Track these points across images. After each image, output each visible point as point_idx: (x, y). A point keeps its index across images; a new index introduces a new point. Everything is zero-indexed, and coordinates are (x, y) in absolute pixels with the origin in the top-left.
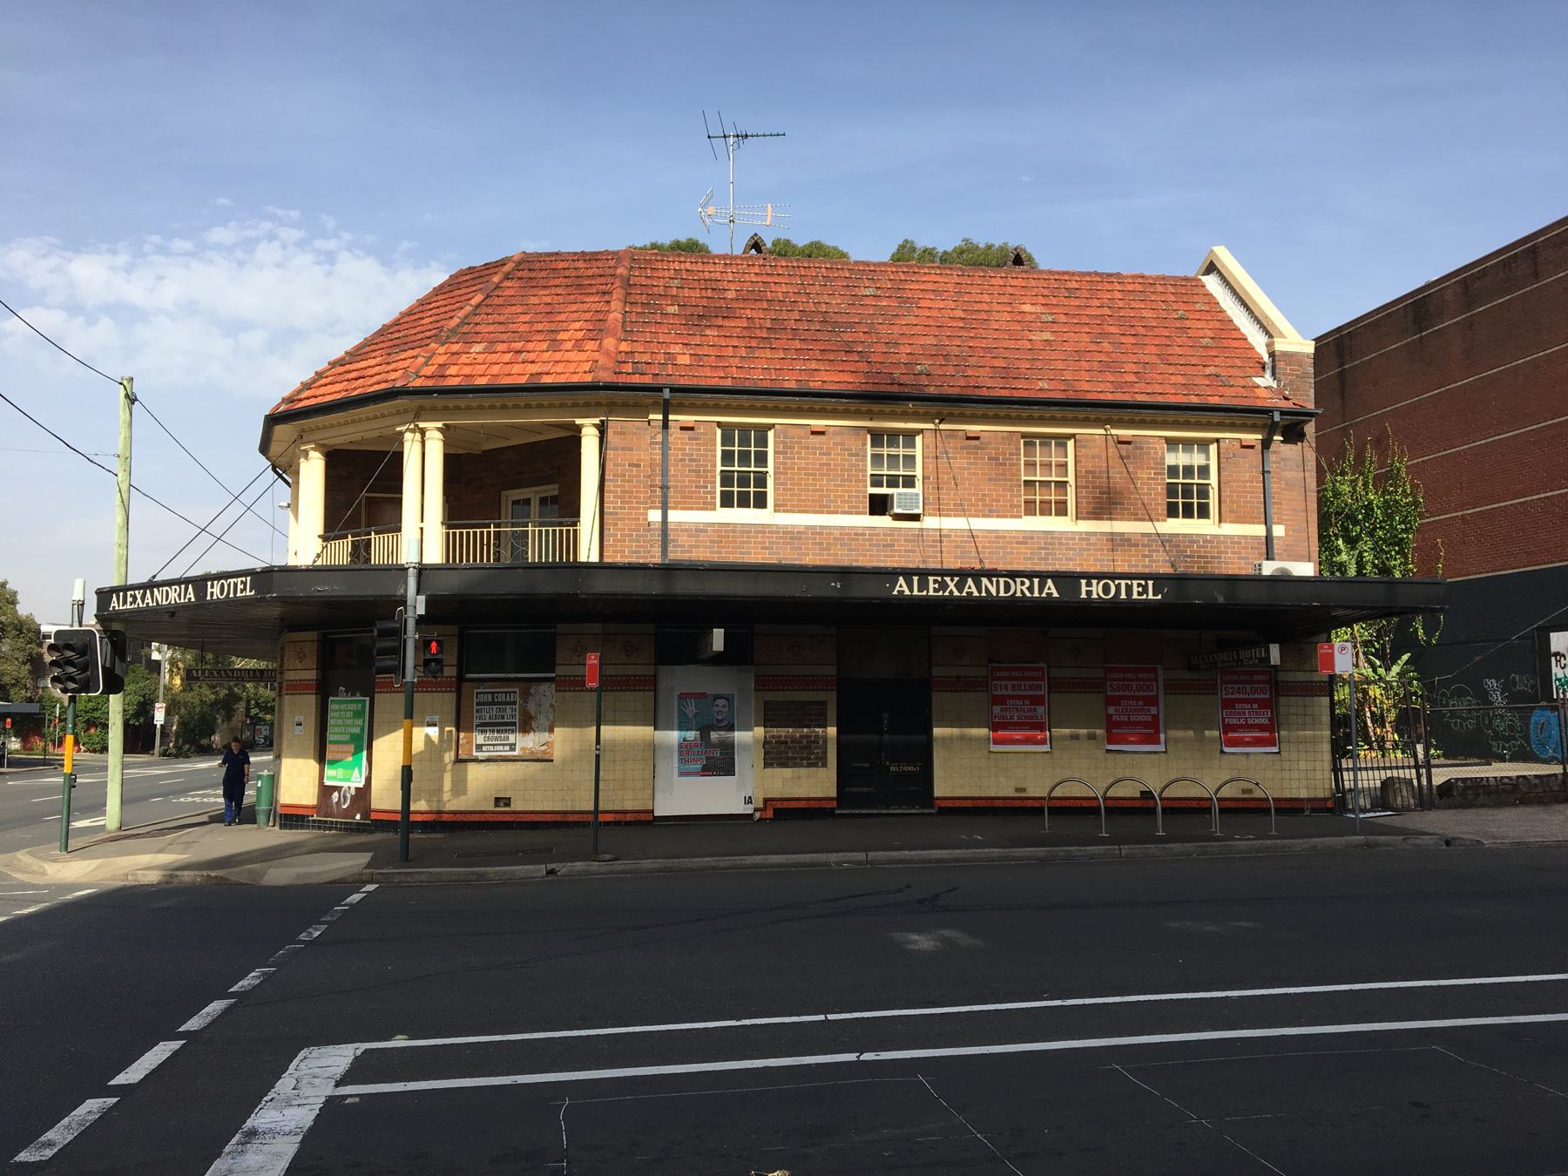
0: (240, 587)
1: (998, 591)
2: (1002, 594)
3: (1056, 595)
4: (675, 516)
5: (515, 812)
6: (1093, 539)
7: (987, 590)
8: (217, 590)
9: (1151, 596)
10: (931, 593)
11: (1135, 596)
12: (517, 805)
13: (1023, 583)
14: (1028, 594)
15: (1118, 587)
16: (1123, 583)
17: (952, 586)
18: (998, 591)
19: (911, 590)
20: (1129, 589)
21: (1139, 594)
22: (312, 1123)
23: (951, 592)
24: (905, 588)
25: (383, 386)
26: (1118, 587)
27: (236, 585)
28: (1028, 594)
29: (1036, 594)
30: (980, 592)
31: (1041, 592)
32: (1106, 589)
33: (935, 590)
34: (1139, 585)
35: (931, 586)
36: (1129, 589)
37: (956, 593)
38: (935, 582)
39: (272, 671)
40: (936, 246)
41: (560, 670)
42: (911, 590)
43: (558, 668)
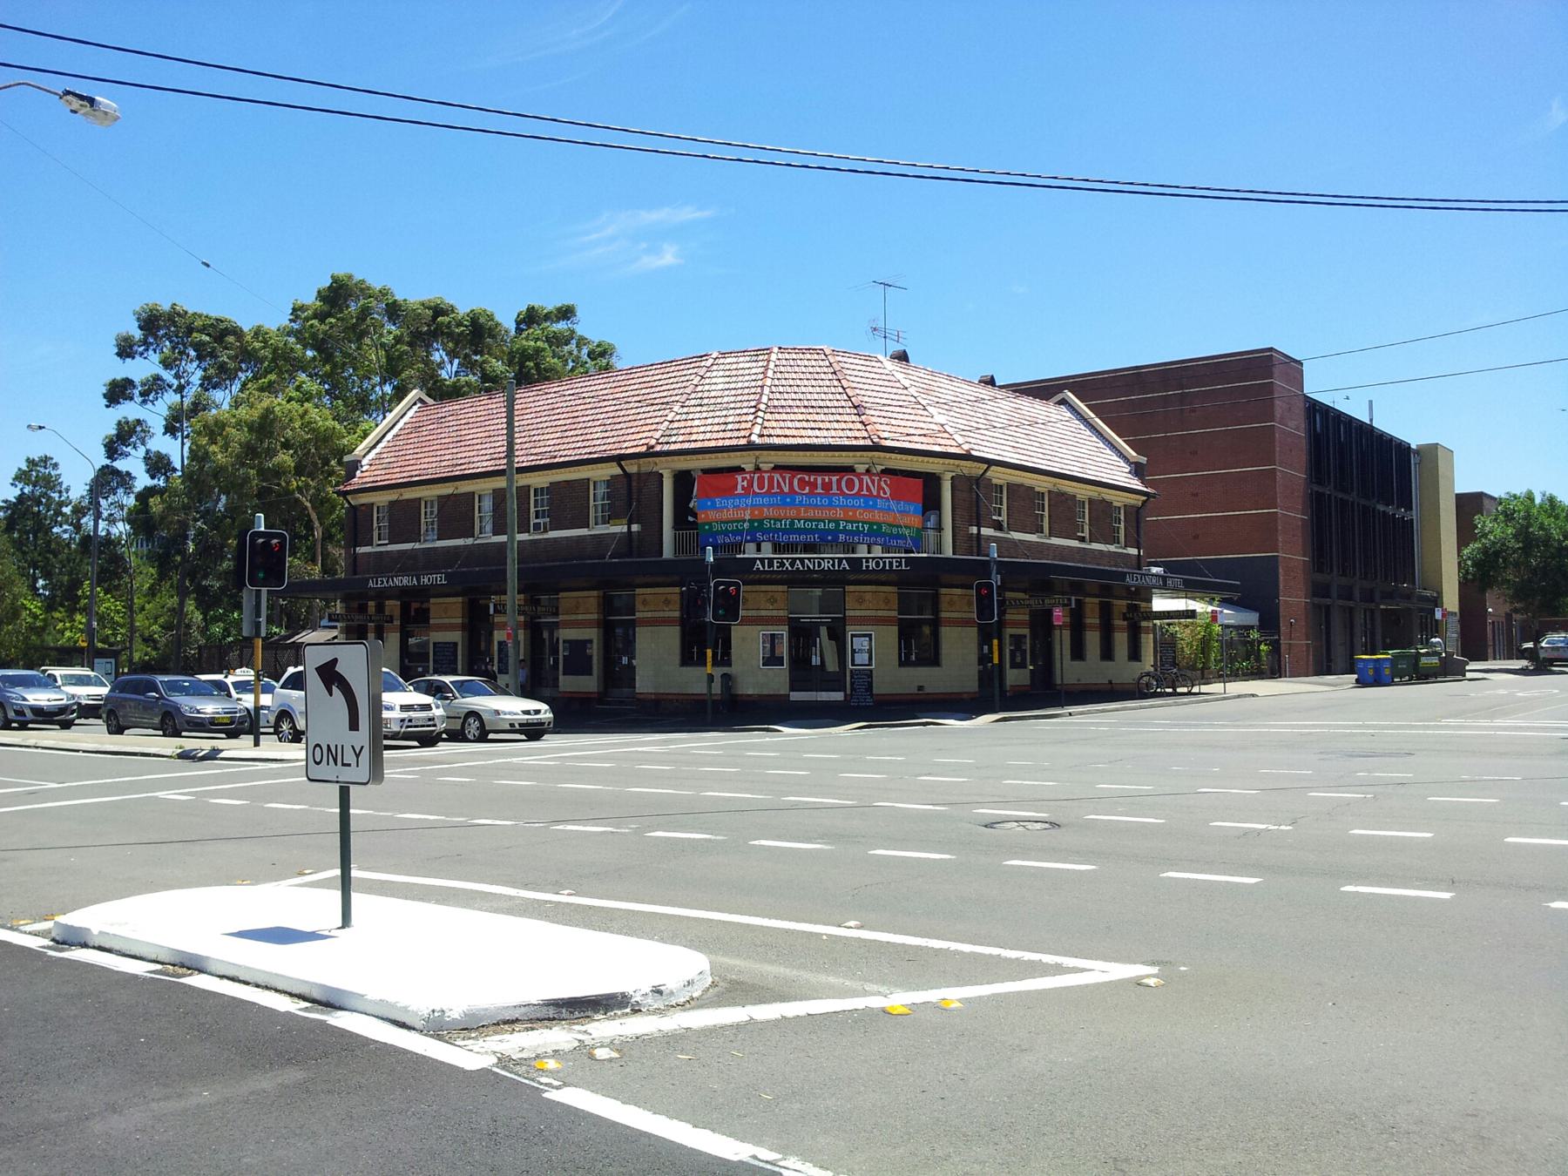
0: (439, 579)
1: (814, 567)
2: (816, 568)
3: (848, 568)
4: (625, 529)
5: (928, 694)
6: (1096, 553)
7: (808, 567)
8: (426, 580)
9: (903, 568)
10: (775, 569)
11: (894, 568)
12: (928, 690)
13: (829, 562)
14: (831, 568)
15: (884, 563)
16: (887, 560)
17: (787, 565)
18: (814, 567)
19: (764, 567)
20: (891, 563)
21: (897, 566)
22: (242, 736)
23: (787, 568)
24: (760, 566)
25: (618, 452)
26: (884, 563)
27: (436, 578)
28: (831, 568)
29: (836, 568)
30: (804, 568)
31: (839, 567)
32: (878, 564)
33: (778, 567)
34: (897, 562)
35: (775, 564)
36: (891, 563)
37: (790, 568)
38: (778, 562)
39: (338, 615)
40: (316, 290)
41: (638, 615)
42: (764, 567)
43: (637, 613)
